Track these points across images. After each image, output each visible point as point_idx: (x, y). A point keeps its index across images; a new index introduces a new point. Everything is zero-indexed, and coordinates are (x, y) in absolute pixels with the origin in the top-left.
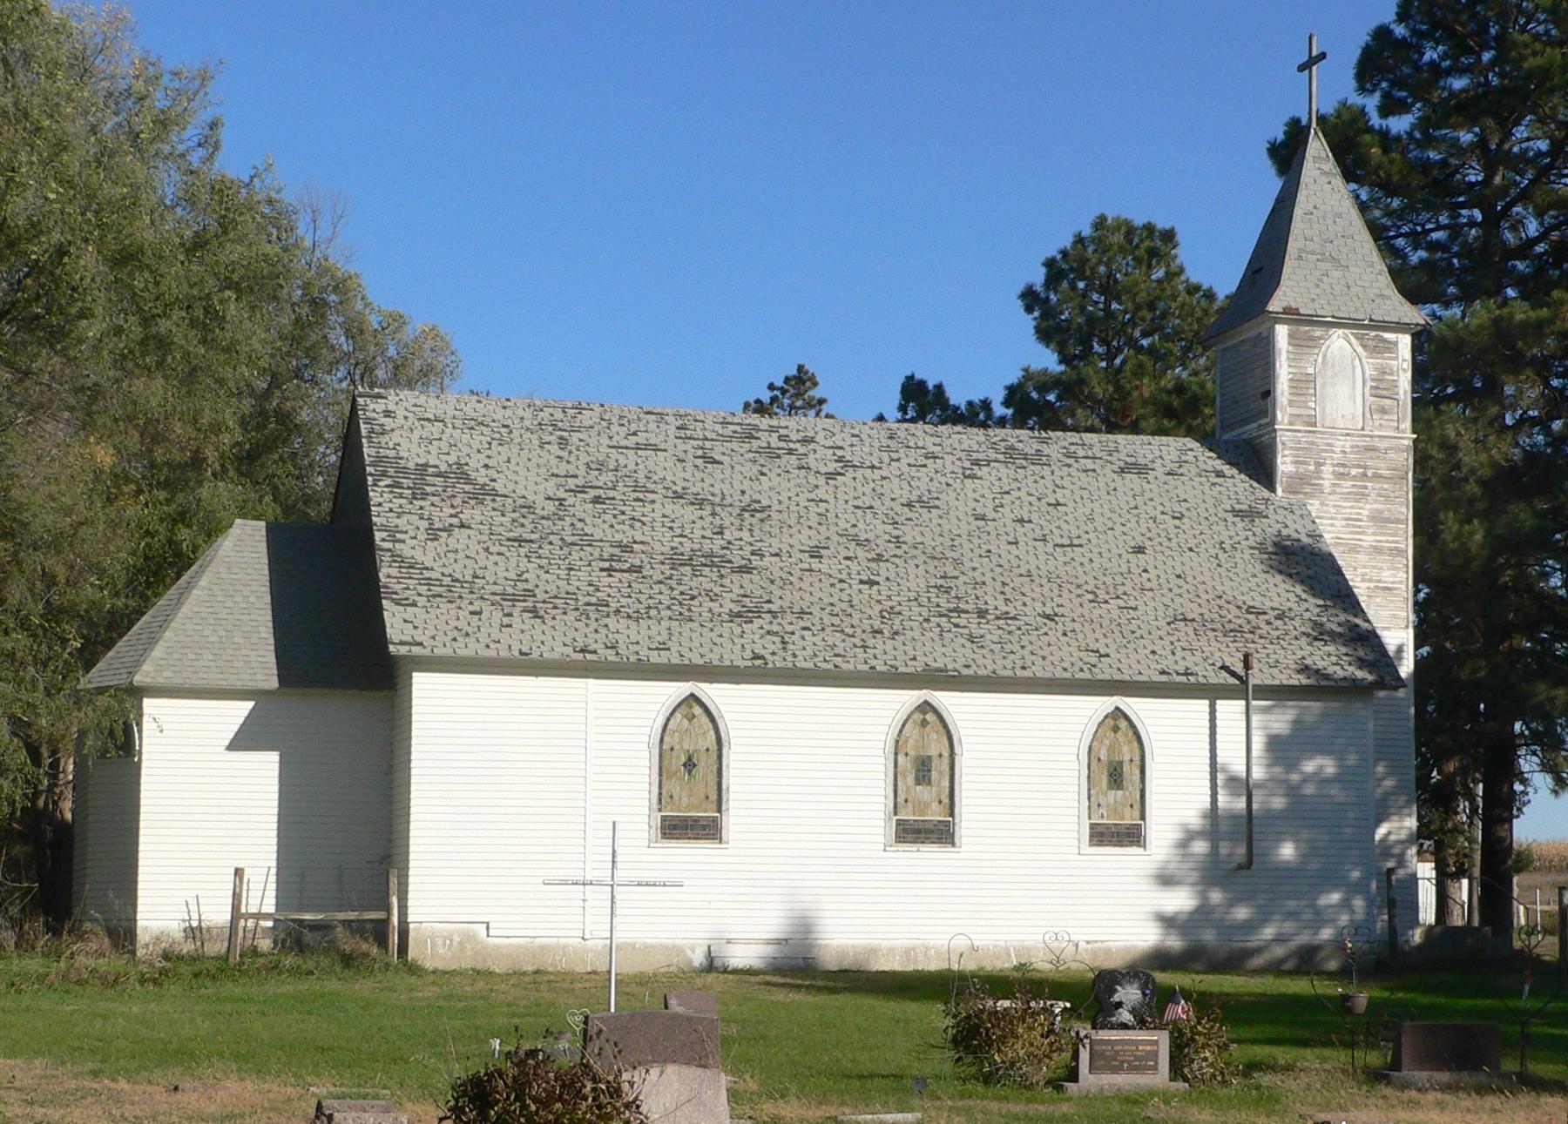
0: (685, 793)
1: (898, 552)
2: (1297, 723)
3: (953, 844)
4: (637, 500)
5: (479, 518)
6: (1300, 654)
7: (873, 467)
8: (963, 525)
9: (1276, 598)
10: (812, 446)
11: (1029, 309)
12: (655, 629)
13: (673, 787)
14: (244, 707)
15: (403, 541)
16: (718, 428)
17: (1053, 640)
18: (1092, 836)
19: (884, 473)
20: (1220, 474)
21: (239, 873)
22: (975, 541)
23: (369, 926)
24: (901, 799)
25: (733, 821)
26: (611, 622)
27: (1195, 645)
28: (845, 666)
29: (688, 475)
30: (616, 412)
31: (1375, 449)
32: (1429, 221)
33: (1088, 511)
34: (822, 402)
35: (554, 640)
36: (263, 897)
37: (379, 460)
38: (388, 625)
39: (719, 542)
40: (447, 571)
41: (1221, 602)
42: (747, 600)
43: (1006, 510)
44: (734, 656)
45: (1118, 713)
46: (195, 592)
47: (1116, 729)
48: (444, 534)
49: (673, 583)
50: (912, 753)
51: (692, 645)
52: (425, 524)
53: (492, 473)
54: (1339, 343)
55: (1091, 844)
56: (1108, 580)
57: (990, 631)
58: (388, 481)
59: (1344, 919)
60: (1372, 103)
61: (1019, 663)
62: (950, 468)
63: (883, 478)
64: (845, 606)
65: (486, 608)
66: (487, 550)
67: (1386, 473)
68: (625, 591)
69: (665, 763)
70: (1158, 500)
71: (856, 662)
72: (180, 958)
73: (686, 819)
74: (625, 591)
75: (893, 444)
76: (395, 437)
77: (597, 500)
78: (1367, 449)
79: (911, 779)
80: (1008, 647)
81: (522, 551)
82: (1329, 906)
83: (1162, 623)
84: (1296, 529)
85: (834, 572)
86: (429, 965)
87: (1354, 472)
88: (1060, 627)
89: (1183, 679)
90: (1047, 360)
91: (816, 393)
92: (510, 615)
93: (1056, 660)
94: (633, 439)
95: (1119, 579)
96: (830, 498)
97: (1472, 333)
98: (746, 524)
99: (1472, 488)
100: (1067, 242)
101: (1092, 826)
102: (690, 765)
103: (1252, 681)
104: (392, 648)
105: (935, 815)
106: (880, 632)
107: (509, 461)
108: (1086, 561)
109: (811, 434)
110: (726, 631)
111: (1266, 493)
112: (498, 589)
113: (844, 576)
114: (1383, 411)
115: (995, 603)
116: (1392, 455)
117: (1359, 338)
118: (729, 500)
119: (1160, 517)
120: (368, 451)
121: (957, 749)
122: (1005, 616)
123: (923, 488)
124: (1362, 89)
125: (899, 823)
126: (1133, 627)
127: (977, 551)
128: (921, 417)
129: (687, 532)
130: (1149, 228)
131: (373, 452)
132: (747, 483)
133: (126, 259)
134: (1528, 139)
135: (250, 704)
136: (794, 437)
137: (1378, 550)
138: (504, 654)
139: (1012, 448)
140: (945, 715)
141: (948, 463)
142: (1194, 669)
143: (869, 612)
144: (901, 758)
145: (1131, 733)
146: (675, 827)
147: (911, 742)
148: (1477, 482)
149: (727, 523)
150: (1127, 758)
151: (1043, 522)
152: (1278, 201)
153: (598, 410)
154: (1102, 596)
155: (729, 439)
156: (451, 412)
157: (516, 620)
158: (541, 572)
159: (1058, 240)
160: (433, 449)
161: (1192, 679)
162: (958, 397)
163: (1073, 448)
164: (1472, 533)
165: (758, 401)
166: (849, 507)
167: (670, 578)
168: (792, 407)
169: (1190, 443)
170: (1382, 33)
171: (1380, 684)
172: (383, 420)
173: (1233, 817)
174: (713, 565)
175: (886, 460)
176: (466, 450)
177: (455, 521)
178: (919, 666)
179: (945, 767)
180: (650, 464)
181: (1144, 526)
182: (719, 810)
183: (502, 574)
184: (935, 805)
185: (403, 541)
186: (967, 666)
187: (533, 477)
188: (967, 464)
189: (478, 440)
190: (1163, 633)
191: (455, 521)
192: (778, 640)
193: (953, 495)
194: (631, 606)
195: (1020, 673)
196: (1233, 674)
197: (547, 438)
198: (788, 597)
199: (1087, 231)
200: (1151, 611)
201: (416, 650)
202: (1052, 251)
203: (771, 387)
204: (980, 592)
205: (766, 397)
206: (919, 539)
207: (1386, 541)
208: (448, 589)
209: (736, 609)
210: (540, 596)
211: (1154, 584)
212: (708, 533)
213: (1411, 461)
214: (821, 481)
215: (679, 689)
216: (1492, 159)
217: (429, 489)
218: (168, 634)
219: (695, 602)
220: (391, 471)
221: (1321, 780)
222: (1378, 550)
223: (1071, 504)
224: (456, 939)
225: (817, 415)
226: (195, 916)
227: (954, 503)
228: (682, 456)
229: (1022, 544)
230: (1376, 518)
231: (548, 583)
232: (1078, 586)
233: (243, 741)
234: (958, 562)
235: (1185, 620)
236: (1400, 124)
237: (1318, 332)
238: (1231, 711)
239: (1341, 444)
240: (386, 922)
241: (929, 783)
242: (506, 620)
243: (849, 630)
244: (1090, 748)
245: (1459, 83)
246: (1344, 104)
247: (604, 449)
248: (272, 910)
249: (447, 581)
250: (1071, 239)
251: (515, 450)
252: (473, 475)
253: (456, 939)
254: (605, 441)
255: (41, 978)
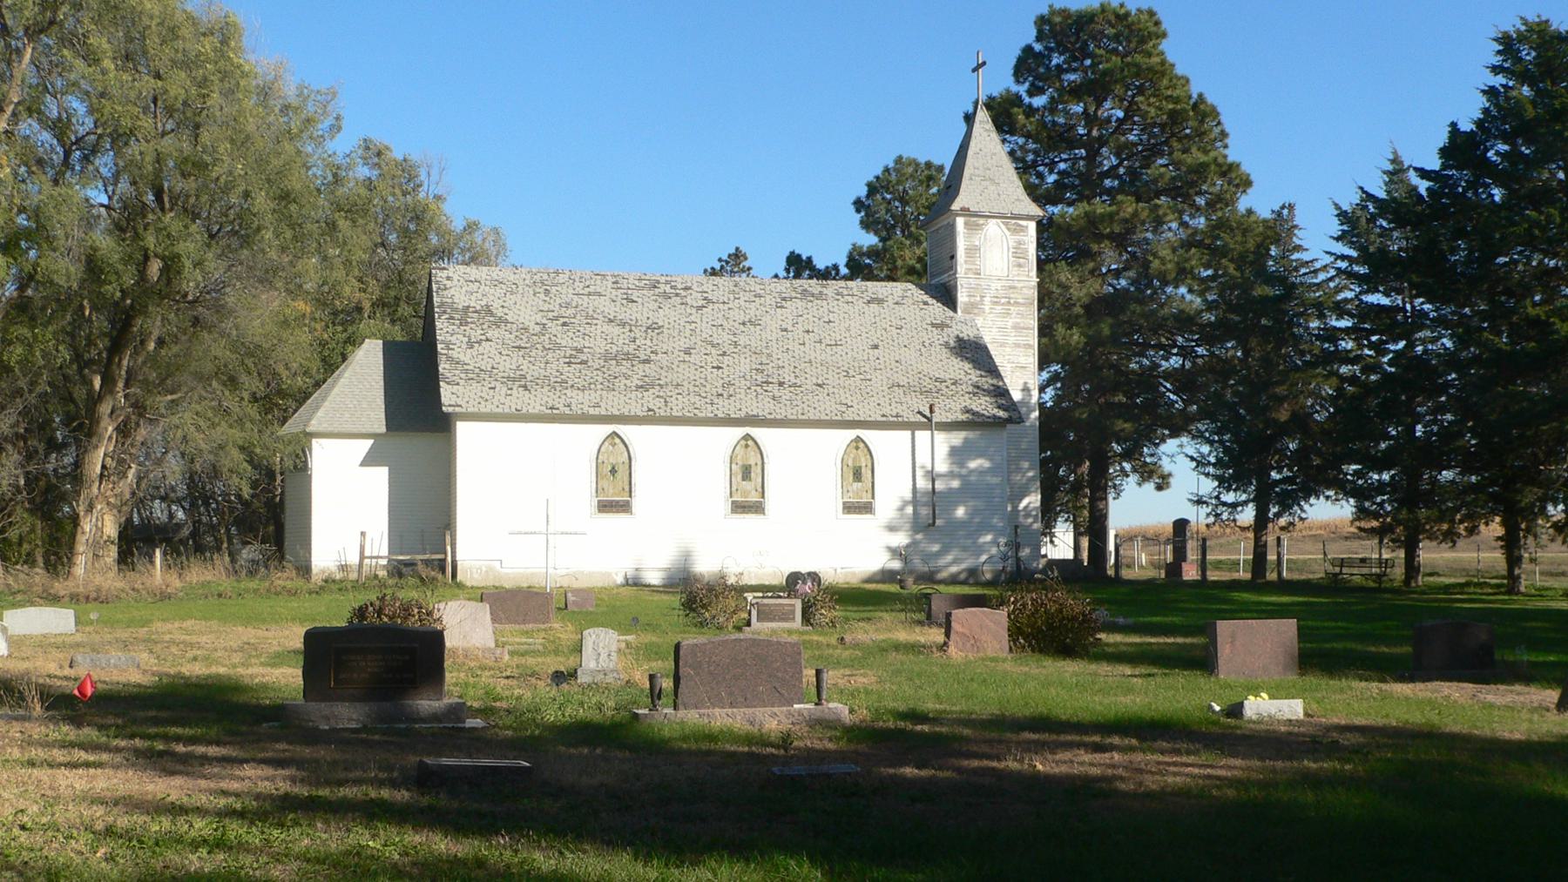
0: (611, 488)
1: (735, 350)
2: (966, 440)
3: (764, 514)
4: (587, 323)
5: (497, 336)
6: (964, 404)
7: (724, 303)
8: (774, 334)
9: (952, 373)
10: (690, 291)
11: (858, 211)
12: (593, 395)
13: (604, 483)
14: (369, 443)
15: (453, 349)
16: (636, 282)
17: (821, 399)
18: (844, 508)
19: (730, 306)
20: (926, 303)
21: (363, 534)
22: (781, 344)
23: (436, 563)
24: (734, 489)
25: (637, 503)
26: (568, 392)
27: (903, 400)
28: (700, 415)
29: (617, 309)
30: (578, 275)
31: (1015, 288)
32: (1056, 157)
33: (847, 325)
34: (749, 269)
35: (535, 402)
36: (379, 546)
37: (442, 304)
38: (442, 395)
39: (633, 346)
40: (477, 365)
41: (921, 376)
42: (646, 379)
43: (800, 326)
44: (639, 411)
45: (859, 439)
46: (342, 380)
47: (857, 448)
48: (477, 345)
49: (605, 370)
50: (740, 463)
51: (614, 404)
52: (467, 339)
53: (506, 310)
54: (993, 228)
55: (844, 513)
56: (856, 364)
57: (785, 394)
58: (447, 316)
59: (994, 550)
60: (1022, 89)
61: (800, 412)
62: (768, 302)
63: (729, 309)
64: (702, 381)
65: (498, 385)
66: (500, 353)
67: (1021, 301)
68: (577, 375)
69: (600, 470)
70: (889, 318)
71: (707, 413)
72: (334, 581)
73: (612, 501)
74: (577, 375)
75: (736, 289)
76: (452, 291)
77: (564, 324)
78: (1011, 288)
79: (740, 477)
80: (796, 402)
81: (520, 353)
82: (985, 543)
83: (885, 388)
84: (967, 333)
85: (697, 362)
86: (469, 584)
87: (1003, 300)
88: (826, 391)
89: (895, 419)
90: (869, 240)
91: (747, 264)
92: (511, 389)
93: (822, 409)
94: (587, 290)
95: (862, 364)
96: (698, 321)
97: (1073, 219)
98: (649, 336)
99: (1078, 310)
100: (879, 171)
101: (844, 503)
102: (613, 471)
103: (934, 420)
104: (444, 408)
105: (754, 498)
106: (722, 395)
107: (515, 303)
108: (844, 354)
109: (689, 285)
110: (633, 395)
111: (952, 314)
112: (506, 375)
113: (703, 364)
114: (1020, 266)
115: (788, 378)
116: (1025, 291)
117: (1006, 224)
118: (640, 323)
119: (889, 328)
120: (436, 299)
121: (766, 460)
122: (795, 385)
123: (752, 314)
124: (1018, 82)
125: (733, 502)
126: (868, 390)
127: (781, 349)
128: (797, 276)
129: (615, 341)
130: (929, 165)
131: (439, 300)
132: (651, 313)
133: (285, 197)
134: (1112, 109)
135: (372, 441)
136: (679, 286)
137: (1017, 345)
138: (507, 410)
139: (806, 290)
140: (758, 441)
141: (768, 300)
142: (901, 414)
143: (716, 384)
144: (734, 466)
145: (866, 450)
146: (605, 506)
147: (739, 457)
148: (1081, 306)
149: (638, 336)
150: (864, 465)
151: (821, 332)
152: (961, 147)
153: (568, 273)
154: (851, 373)
155: (643, 288)
156: (484, 276)
157: (514, 392)
158: (530, 365)
159: (874, 170)
160: (473, 298)
161: (900, 419)
162: (820, 263)
163: (841, 290)
164: (1072, 335)
165: (713, 268)
166: (709, 325)
167: (604, 367)
168: (732, 271)
169: (910, 286)
170: (1028, 50)
171: (1009, 420)
172: (446, 282)
173: (926, 493)
174: (629, 359)
175: (732, 298)
176: (492, 298)
177: (483, 338)
178: (743, 414)
179: (759, 470)
180: (596, 303)
181: (879, 333)
182: (630, 496)
183: (508, 366)
184: (753, 492)
185: (453, 349)
186: (770, 414)
187: (529, 311)
188: (779, 300)
189: (499, 291)
190: (885, 394)
191: (483, 338)
192: (662, 400)
193: (769, 317)
194: (581, 383)
195: (800, 417)
196: (924, 416)
197: (538, 290)
198: (670, 376)
199: (891, 165)
200: (879, 381)
201: (457, 409)
202: (871, 178)
203: (720, 260)
204: (781, 372)
205: (717, 266)
206: (748, 343)
207: (1022, 341)
208: (476, 376)
209: (640, 383)
210: (529, 378)
211: (882, 367)
212: (627, 342)
213: (1036, 293)
214: (694, 311)
215: (608, 429)
216: (1090, 119)
217: (469, 320)
218: (326, 403)
219: (617, 380)
220: (449, 310)
221: (981, 472)
222: (1017, 345)
223: (837, 322)
224: (484, 569)
225: (748, 276)
226: (343, 558)
227: (769, 322)
228: (615, 298)
229: (807, 345)
230: (1016, 327)
231: (532, 371)
232: (839, 368)
233: (370, 460)
234: (769, 355)
235: (899, 386)
236: (1039, 101)
237: (981, 221)
238: (923, 436)
239: (996, 285)
240: (444, 560)
241: (750, 480)
242: (509, 392)
243: (704, 395)
244: (843, 459)
245: (1072, 77)
246: (1008, 91)
247: (570, 296)
248: (387, 554)
249: (477, 370)
250: (882, 169)
251: (519, 296)
252: (495, 311)
253: (484, 569)
254: (571, 291)
255: (256, 591)
